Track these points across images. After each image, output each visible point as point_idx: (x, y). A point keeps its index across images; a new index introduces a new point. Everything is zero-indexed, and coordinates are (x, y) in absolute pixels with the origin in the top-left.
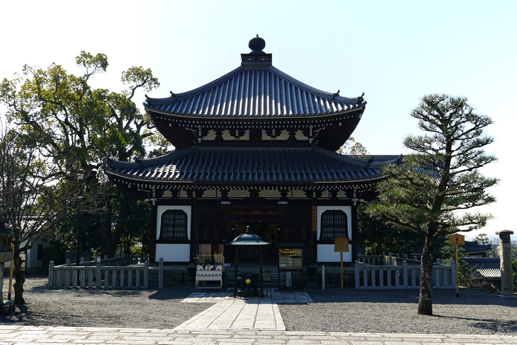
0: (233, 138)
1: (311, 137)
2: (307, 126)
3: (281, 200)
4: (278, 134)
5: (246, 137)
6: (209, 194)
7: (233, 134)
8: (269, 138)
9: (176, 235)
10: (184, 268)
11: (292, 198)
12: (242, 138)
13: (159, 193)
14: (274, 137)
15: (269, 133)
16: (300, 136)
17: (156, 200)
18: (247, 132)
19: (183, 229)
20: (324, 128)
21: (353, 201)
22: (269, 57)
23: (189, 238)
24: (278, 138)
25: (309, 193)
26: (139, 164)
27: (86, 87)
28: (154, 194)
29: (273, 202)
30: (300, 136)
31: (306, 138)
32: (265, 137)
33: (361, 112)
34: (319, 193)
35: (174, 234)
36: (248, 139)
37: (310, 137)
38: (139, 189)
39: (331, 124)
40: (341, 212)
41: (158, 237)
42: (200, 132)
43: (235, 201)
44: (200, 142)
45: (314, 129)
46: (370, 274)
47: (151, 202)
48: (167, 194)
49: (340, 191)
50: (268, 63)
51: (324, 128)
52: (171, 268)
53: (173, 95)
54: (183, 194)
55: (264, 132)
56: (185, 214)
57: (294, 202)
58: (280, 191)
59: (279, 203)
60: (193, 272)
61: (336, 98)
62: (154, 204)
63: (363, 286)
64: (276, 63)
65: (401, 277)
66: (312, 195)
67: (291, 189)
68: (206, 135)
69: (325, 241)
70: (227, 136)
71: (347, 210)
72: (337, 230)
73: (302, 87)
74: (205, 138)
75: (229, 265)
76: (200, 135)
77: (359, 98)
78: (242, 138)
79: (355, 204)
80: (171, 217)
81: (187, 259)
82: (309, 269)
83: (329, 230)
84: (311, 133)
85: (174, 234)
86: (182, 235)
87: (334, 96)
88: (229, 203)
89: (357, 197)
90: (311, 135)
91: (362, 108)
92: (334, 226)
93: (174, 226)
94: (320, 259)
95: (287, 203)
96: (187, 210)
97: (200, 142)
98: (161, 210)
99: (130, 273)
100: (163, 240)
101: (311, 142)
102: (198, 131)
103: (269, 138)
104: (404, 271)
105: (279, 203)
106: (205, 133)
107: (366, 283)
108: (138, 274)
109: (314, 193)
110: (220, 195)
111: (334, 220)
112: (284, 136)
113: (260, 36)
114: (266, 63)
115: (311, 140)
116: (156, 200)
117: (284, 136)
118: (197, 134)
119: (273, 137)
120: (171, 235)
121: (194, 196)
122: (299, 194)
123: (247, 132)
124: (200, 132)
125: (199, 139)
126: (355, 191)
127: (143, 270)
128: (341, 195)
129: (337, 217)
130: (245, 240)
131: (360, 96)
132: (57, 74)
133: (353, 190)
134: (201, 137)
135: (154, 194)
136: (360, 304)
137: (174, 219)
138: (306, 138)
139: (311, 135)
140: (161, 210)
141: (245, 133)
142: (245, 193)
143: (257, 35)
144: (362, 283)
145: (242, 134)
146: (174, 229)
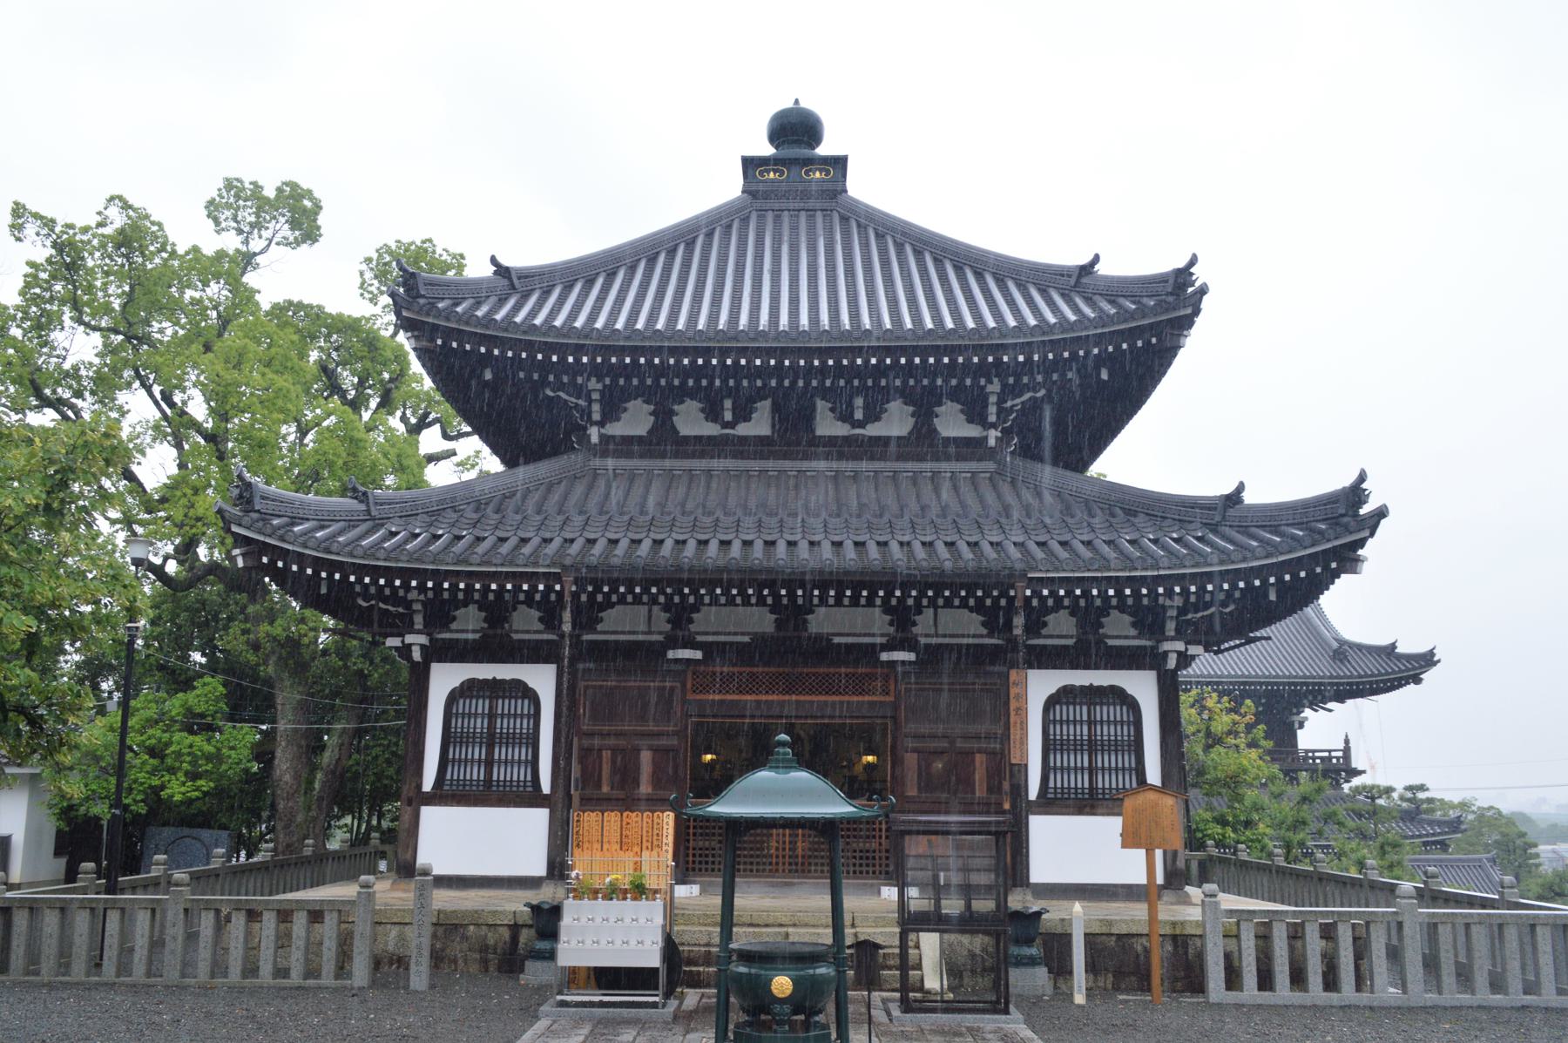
0: (712, 429)
1: (994, 426)
4: (873, 415)
5: (759, 425)
6: (625, 623)
7: (713, 414)
8: (842, 430)
9: (498, 773)
12: (743, 429)
13: (440, 613)
16: (951, 424)
18: (764, 408)
19: (523, 753)
23: (546, 788)
24: (873, 430)
26: (363, 507)
27: (244, 297)
28: (419, 621)
31: (973, 431)
32: (828, 425)
33: (1186, 323)
34: (1035, 625)
35: (489, 772)
37: (987, 426)
40: (1118, 695)
41: (428, 785)
42: (596, 407)
43: (931, 657)
44: (595, 439)
45: (1007, 392)
46: (1264, 938)
47: (405, 650)
49: (1115, 613)
53: (502, 271)
56: (1133, 706)
59: (884, 656)
60: (547, 920)
62: (417, 655)
64: (861, 187)
65: (1394, 954)
66: (1009, 625)
70: (690, 421)
71: (1142, 687)
73: (957, 254)
76: (596, 417)
78: (743, 429)
79: (1172, 663)
80: (482, 706)
81: (536, 866)
83: (1071, 760)
84: (993, 409)
85: (489, 772)
86: (520, 774)
87: (1080, 276)
88: (698, 655)
90: (992, 418)
92: (1093, 746)
93: (491, 740)
94: (1042, 870)
95: (911, 657)
96: (542, 679)
97: (595, 439)
98: (444, 679)
100: (446, 794)
101: (992, 442)
104: (1407, 930)
105: (884, 656)
106: (612, 411)
108: (328, 930)
109: (1019, 621)
113: (803, 104)
115: (993, 436)
117: (896, 422)
119: (726, 425)
120: (476, 773)
121: (567, 627)
123: (764, 408)
124: (596, 407)
128: (1119, 630)
129: (1102, 712)
132: (134, 237)
134: (601, 424)
135: (419, 621)
137: (492, 716)
138: (973, 431)
139: (992, 418)
140: (444, 679)
142: (762, 621)
143: (797, 101)
144: (1233, 979)
145: (743, 414)
146: (490, 752)
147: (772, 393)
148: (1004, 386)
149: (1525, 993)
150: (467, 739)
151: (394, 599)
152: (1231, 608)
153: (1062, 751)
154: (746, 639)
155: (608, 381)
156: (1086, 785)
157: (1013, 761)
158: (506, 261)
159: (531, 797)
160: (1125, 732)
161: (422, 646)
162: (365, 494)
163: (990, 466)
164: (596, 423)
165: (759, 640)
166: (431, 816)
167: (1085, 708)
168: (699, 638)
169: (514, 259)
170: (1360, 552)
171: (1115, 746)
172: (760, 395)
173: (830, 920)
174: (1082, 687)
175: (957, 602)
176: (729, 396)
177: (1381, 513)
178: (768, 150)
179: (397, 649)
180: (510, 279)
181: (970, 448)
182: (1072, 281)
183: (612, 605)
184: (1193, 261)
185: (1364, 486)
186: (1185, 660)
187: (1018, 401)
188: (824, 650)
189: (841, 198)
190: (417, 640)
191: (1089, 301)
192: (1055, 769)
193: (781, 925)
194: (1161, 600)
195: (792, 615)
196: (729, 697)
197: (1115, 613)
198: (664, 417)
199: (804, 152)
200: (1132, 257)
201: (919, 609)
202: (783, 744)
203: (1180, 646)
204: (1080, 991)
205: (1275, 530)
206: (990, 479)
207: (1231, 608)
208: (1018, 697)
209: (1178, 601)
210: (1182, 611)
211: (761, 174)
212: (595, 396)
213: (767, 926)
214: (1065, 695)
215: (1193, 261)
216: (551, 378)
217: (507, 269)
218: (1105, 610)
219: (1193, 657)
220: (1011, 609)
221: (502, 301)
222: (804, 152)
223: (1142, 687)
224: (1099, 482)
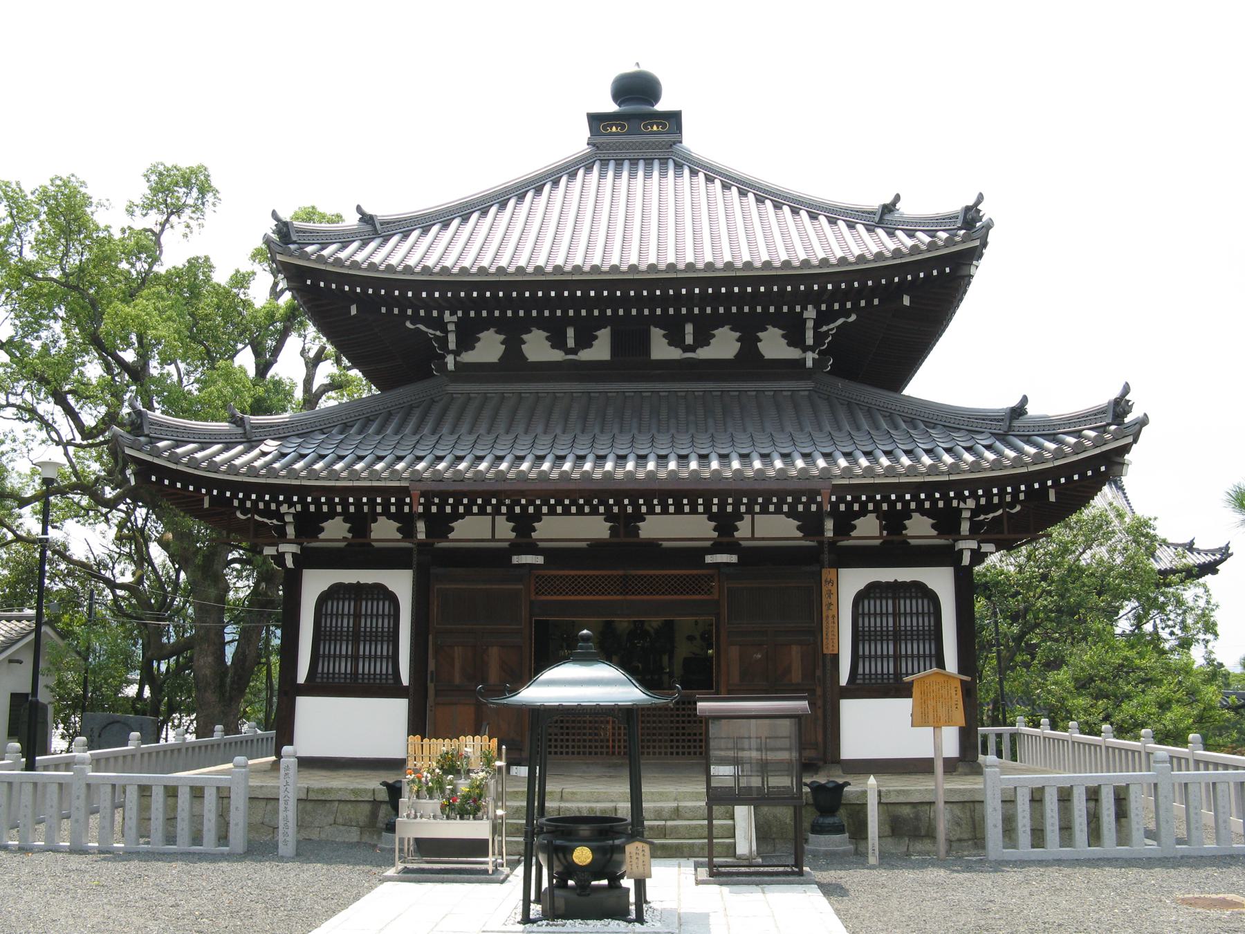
0: (557, 356)
1: (812, 349)
2: (798, 309)
3: (717, 548)
4: (703, 339)
5: (600, 350)
6: (471, 530)
7: (557, 341)
8: (675, 354)
9: (364, 667)
10: (373, 783)
11: (753, 538)
12: (585, 355)
13: (309, 525)
14: (692, 349)
15: (675, 339)
16: (773, 345)
17: (294, 548)
18: (604, 335)
20: (853, 318)
21: (961, 551)
22: (673, 119)
23: (405, 680)
24: (703, 353)
25: (810, 524)
26: (240, 431)
28: (290, 531)
29: (691, 555)
30: (773, 345)
31: (793, 353)
32: (661, 349)
33: (974, 254)
34: (845, 524)
37: (805, 349)
38: (239, 515)
39: (876, 302)
42: (452, 338)
43: (558, 556)
44: (451, 366)
45: (821, 319)
47: (280, 558)
48: (335, 531)
49: (916, 515)
50: (671, 138)
51: (853, 318)
52: (339, 782)
53: (367, 219)
54: (384, 531)
55: (657, 334)
56: (393, 599)
57: (761, 559)
58: (712, 517)
59: (709, 559)
61: (887, 217)
62: (289, 563)
63: (1014, 846)
66: (821, 530)
67: (750, 511)
68: (473, 348)
69: (864, 688)
70: (537, 347)
71: (940, 581)
72: (907, 648)
74: (468, 357)
76: (452, 345)
77: (968, 209)
78: (585, 355)
79: (966, 560)
80: (347, 607)
82: (817, 789)
86: (382, 667)
87: (883, 214)
88: (539, 560)
89: (975, 529)
90: (810, 341)
91: (977, 243)
92: (897, 636)
93: (356, 636)
94: (851, 749)
95: (733, 559)
96: (400, 583)
97: (451, 366)
98: (315, 583)
99: (184, 797)
100: (319, 686)
101: (809, 364)
102: (446, 332)
103: (675, 354)
105: (709, 559)
106: (467, 340)
107: (1024, 836)
108: (210, 798)
109: (829, 525)
110: (505, 530)
111: (896, 615)
112: (724, 345)
114: (666, 138)
115: (810, 358)
116: (294, 548)
117: (724, 345)
118: (444, 342)
119: (687, 349)
120: (344, 667)
122: (777, 528)
123: (604, 335)
124: (452, 338)
125: (450, 360)
126: (966, 514)
127: (201, 789)
128: (919, 528)
129: (906, 605)
130: (581, 683)
131: (971, 203)
133: (959, 511)
134: (457, 353)
135: (290, 531)
137: (357, 616)
138: (793, 353)
139: (810, 341)
141: (596, 338)
142: (596, 528)
145: (585, 340)
147: (614, 322)
148: (819, 312)
149: (1033, 846)
151: (267, 513)
152: (1018, 508)
153: (876, 641)
154: (584, 544)
155: (460, 313)
156: (891, 671)
158: (369, 210)
159: (389, 688)
160: (927, 622)
161: (294, 555)
162: (242, 419)
163: (809, 385)
164: (452, 352)
165: (596, 546)
166: (306, 706)
167: (890, 602)
168: (541, 544)
169: (382, 210)
170: (1127, 457)
171: (916, 635)
172: (602, 322)
174: (887, 583)
175: (475, 509)
176: (570, 325)
177: (1144, 421)
178: (611, 107)
179: (273, 557)
180: (374, 225)
181: (792, 368)
182: (877, 219)
183: (462, 516)
184: (980, 198)
185: (1128, 398)
186: (978, 557)
187: (831, 326)
188: (654, 552)
189: (677, 146)
190: (289, 549)
191: (891, 234)
192: (864, 657)
194: (955, 503)
195: (625, 523)
196: (628, 597)
197: (916, 515)
199: (645, 108)
200: (931, 198)
201: (739, 516)
202: (586, 639)
203: (973, 544)
204: (183, 820)
205: (1053, 438)
206: (809, 397)
207: (1018, 508)
208: (830, 593)
209: (971, 503)
210: (975, 512)
211: (645, 127)
212: (451, 327)
214: (872, 591)
215: (980, 198)
216: (409, 312)
217: (371, 217)
218: (907, 514)
219: (986, 555)
220: (820, 516)
221: (365, 244)
222: (645, 108)
223: (940, 581)
224: (910, 399)
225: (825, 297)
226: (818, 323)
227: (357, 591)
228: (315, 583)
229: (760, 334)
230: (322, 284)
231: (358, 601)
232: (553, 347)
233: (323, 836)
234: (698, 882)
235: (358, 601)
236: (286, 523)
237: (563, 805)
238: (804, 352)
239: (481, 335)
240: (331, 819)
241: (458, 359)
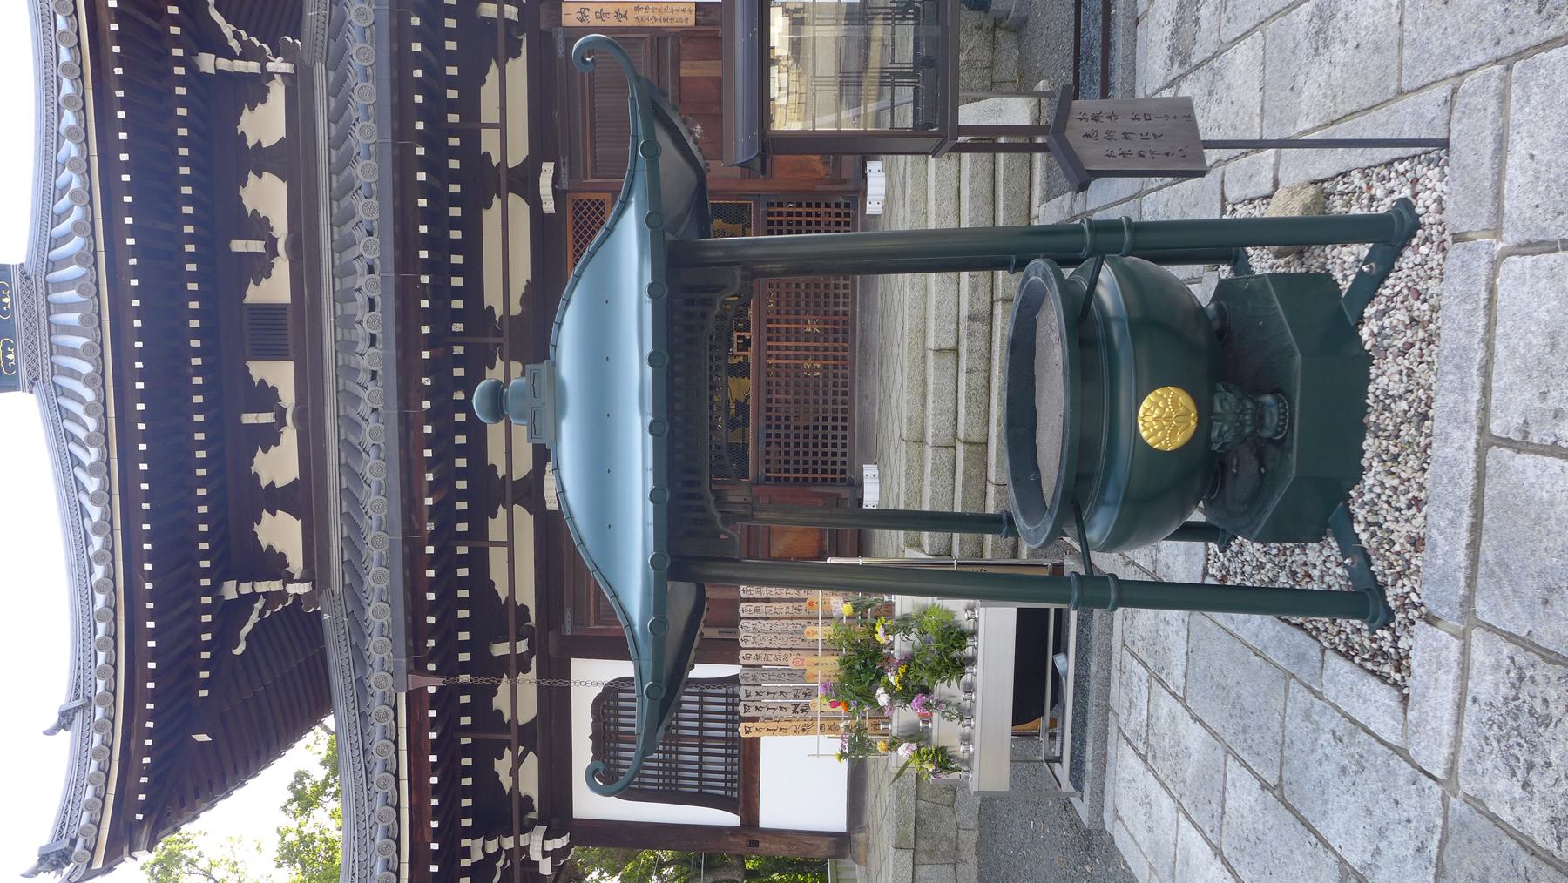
0: (290, 436)
4: (258, 226)
5: (280, 375)
7: (270, 437)
8: (282, 267)
12: (288, 397)
14: (272, 243)
15: (260, 267)
16: (265, 123)
18: (259, 370)
24: (280, 227)
31: (277, 93)
32: (275, 288)
36: (289, 367)
41: (731, 819)
42: (262, 587)
55: (256, 294)
59: (549, 207)
62: (559, 843)
68: (282, 556)
74: (296, 563)
75: (870, 471)
76: (275, 586)
78: (288, 397)
84: (240, 66)
90: (253, 67)
98: (590, 804)
102: (254, 596)
103: (282, 267)
105: (549, 207)
106: (274, 565)
115: (278, 65)
117: (267, 196)
123: (259, 370)
134: (289, 579)
136: (1242, 616)
138: (277, 93)
139: (253, 67)
145: (266, 397)
150: (672, 770)
157: (692, 22)
158: (54, 719)
161: (547, 837)
166: (772, 814)
173: (953, 275)
181: (299, 91)
190: (536, 844)
193: (924, 357)
198: (278, 499)
213: (924, 381)
217: (63, 714)
225: (436, 183)
226: (224, 51)
227: (604, 738)
228: (590, 804)
229: (251, 144)
230: (142, 797)
231: (618, 738)
232: (277, 443)
233: (972, 824)
234: (285, 809)
235: (618, 738)
236: (500, 849)
237: (929, 440)
238: (271, 76)
239: (264, 545)
240: (945, 812)
241: (296, 577)
